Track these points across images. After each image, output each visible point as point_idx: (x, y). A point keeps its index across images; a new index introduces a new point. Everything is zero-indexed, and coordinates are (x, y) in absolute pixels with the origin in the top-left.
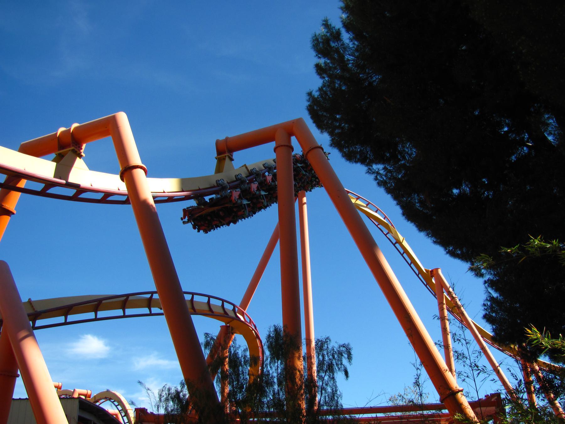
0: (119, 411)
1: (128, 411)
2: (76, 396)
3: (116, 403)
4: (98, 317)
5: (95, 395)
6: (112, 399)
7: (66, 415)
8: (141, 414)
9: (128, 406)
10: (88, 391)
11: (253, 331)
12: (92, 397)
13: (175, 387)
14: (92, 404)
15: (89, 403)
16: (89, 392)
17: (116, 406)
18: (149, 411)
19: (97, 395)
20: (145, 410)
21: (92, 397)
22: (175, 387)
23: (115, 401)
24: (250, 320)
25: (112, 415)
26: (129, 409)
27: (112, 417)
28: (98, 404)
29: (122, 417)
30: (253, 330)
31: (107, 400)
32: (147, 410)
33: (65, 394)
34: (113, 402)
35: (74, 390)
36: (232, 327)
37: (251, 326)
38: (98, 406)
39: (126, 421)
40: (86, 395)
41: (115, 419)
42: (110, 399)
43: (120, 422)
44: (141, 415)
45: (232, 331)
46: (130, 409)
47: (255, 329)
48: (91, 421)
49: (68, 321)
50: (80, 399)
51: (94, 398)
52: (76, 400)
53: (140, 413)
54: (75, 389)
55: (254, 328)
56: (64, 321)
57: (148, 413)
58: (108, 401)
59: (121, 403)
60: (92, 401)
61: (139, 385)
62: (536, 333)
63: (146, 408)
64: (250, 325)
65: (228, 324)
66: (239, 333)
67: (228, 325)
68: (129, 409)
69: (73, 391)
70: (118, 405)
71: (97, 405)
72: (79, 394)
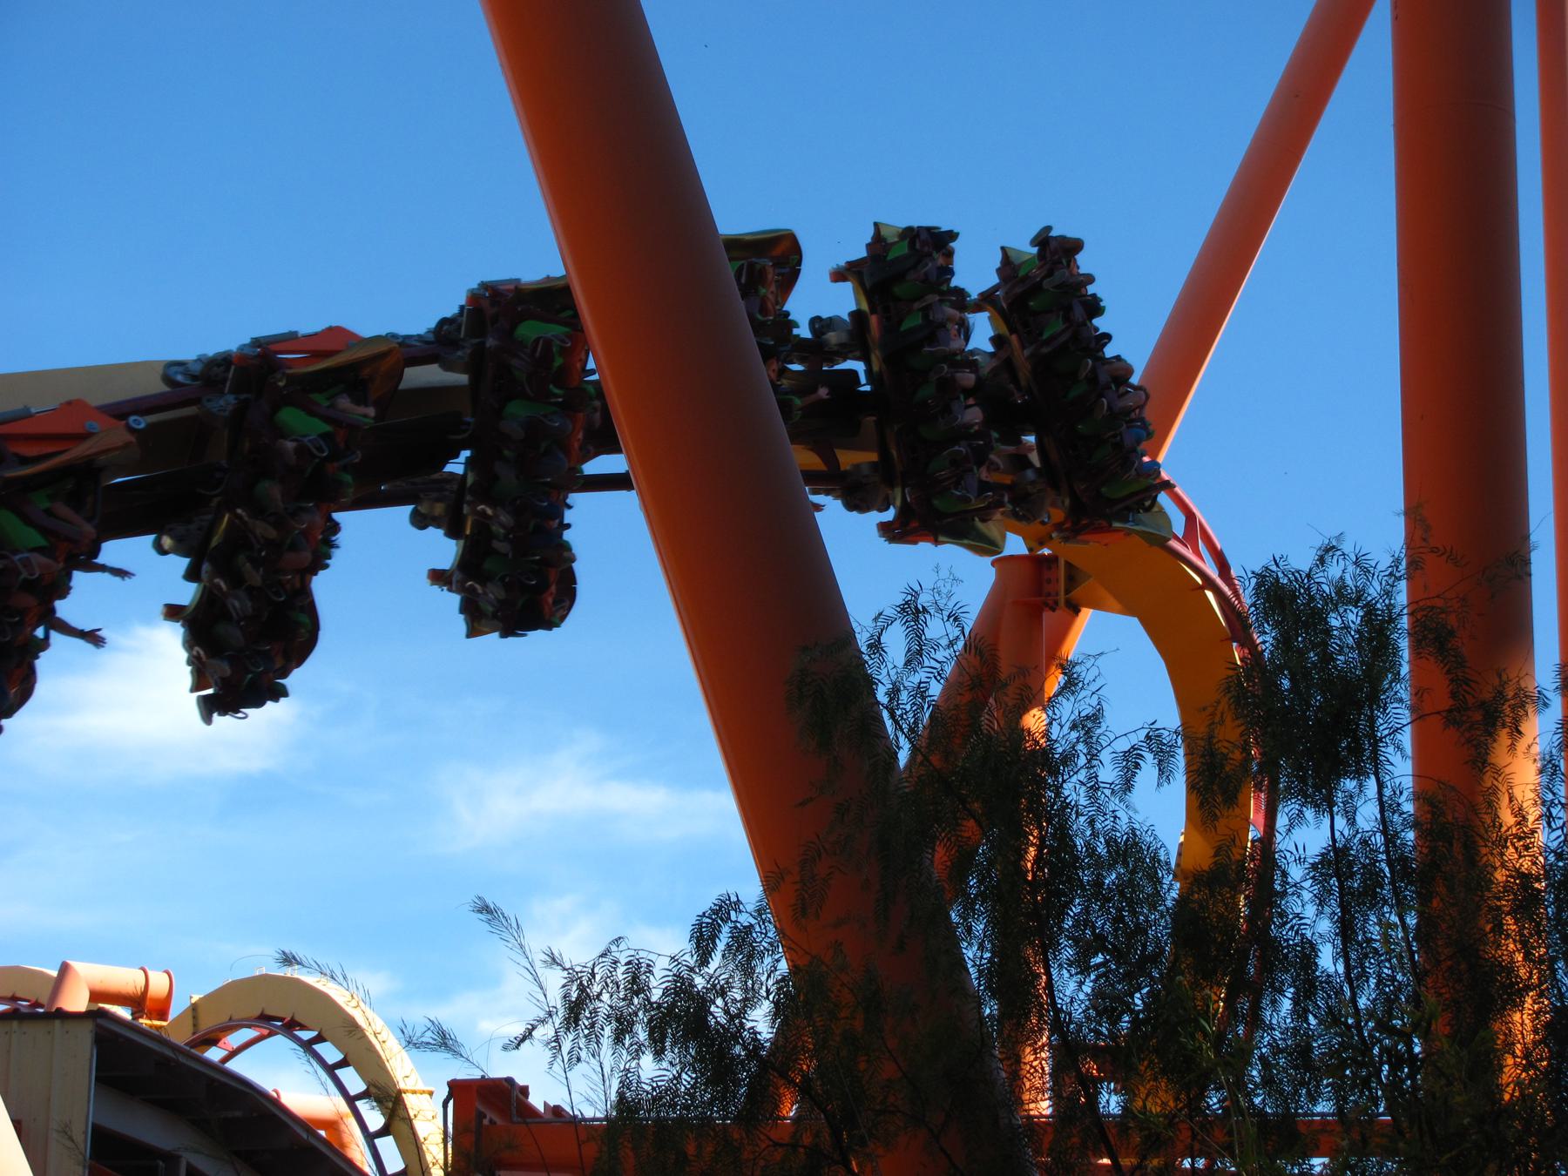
0: (351, 1100)
1: (408, 1099)
2: (76, 1001)
3: (331, 1053)
4: (378, 1142)
5: (195, 998)
6: (303, 1027)
7: (18, 1125)
8: (490, 1115)
9: (403, 1068)
10: (150, 973)
11: (1210, 595)
12: (175, 1011)
13: (673, 958)
14: (182, 1059)
15: (169, 1053)
16: (159, 984)
17: (331, 1070)
18: (537, 1100)
19: (209, 998)
20: (516, 1093)
21: (174, 1013)
22: (673, 958)
23: (320, 1039)
24: (1190, 517)
25: (308, 1125)
26: (414, 1092)
27: (305, 1136)
28: (214, 1054)
29: (370, 1137)
30: (1209, 583)
31: (271, 1034)
32: (525, 1091)
33: (9, 995)
34: (307, 1046)
35: (65, 969)
36: (1069, 565)
37: (1199, 563)
38: (218, 1068)
39: (394, 1163)
40: (138, 1002)
41: (323, 1149)
42: (290, 1027)
43: (351, 1163)
44: (486, 1122)
45: (1067, 592)
46: (420, 1086)
47: (1219, 582)
48: (171, 1158)
49: (339, 1072)
50: (101, 1021)
51: (190, 1022)
52: (71, 1026)
53: (482, 1108)
54: (72, 963)
55: (1213, 572)
56: (352, 1092)
57: (532, 1111)
58: (280, 1042)
59: (349, 1033)
60: (180, 1038)
61: (478, 922)
62: (1398, 926)
63: (521, 1081)
64: (1188, 553)
65: (1042, 544)
66: (1112, 601)
67: (1046, 552)
68: (414, 1092)
69: (54, 973)
70: (343, 1063)
71: (208, 1064)
72: (96, 996)
